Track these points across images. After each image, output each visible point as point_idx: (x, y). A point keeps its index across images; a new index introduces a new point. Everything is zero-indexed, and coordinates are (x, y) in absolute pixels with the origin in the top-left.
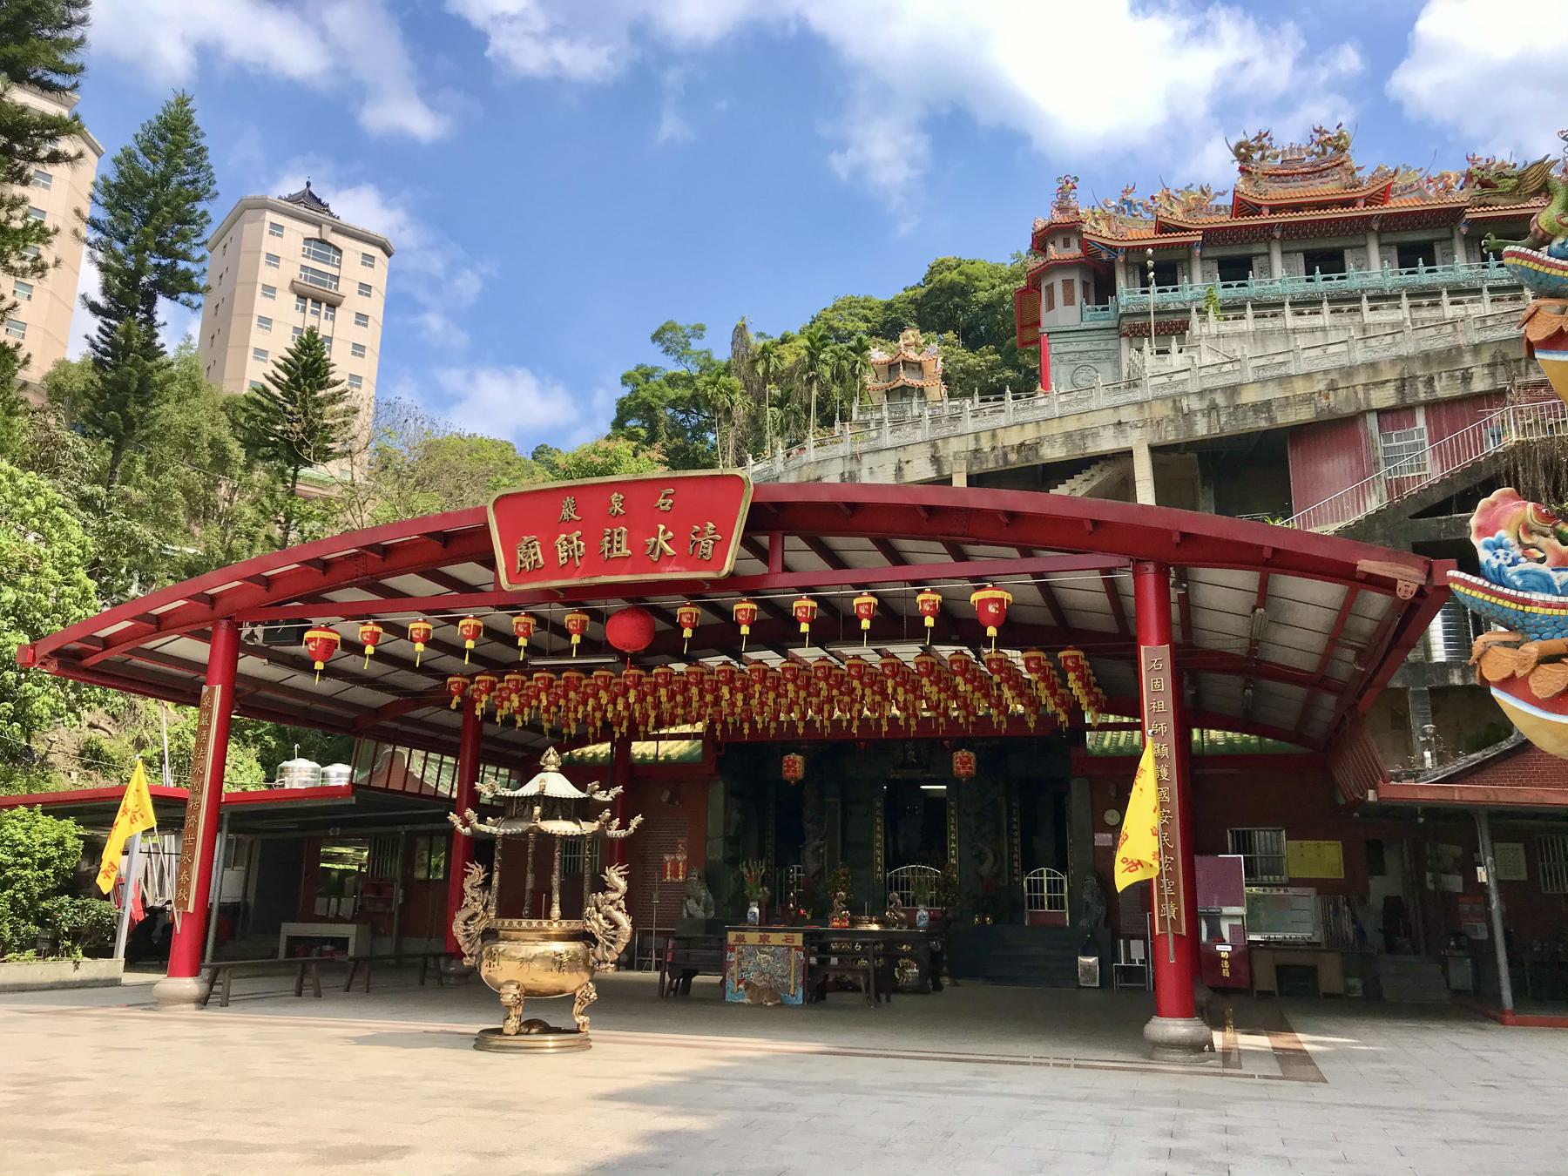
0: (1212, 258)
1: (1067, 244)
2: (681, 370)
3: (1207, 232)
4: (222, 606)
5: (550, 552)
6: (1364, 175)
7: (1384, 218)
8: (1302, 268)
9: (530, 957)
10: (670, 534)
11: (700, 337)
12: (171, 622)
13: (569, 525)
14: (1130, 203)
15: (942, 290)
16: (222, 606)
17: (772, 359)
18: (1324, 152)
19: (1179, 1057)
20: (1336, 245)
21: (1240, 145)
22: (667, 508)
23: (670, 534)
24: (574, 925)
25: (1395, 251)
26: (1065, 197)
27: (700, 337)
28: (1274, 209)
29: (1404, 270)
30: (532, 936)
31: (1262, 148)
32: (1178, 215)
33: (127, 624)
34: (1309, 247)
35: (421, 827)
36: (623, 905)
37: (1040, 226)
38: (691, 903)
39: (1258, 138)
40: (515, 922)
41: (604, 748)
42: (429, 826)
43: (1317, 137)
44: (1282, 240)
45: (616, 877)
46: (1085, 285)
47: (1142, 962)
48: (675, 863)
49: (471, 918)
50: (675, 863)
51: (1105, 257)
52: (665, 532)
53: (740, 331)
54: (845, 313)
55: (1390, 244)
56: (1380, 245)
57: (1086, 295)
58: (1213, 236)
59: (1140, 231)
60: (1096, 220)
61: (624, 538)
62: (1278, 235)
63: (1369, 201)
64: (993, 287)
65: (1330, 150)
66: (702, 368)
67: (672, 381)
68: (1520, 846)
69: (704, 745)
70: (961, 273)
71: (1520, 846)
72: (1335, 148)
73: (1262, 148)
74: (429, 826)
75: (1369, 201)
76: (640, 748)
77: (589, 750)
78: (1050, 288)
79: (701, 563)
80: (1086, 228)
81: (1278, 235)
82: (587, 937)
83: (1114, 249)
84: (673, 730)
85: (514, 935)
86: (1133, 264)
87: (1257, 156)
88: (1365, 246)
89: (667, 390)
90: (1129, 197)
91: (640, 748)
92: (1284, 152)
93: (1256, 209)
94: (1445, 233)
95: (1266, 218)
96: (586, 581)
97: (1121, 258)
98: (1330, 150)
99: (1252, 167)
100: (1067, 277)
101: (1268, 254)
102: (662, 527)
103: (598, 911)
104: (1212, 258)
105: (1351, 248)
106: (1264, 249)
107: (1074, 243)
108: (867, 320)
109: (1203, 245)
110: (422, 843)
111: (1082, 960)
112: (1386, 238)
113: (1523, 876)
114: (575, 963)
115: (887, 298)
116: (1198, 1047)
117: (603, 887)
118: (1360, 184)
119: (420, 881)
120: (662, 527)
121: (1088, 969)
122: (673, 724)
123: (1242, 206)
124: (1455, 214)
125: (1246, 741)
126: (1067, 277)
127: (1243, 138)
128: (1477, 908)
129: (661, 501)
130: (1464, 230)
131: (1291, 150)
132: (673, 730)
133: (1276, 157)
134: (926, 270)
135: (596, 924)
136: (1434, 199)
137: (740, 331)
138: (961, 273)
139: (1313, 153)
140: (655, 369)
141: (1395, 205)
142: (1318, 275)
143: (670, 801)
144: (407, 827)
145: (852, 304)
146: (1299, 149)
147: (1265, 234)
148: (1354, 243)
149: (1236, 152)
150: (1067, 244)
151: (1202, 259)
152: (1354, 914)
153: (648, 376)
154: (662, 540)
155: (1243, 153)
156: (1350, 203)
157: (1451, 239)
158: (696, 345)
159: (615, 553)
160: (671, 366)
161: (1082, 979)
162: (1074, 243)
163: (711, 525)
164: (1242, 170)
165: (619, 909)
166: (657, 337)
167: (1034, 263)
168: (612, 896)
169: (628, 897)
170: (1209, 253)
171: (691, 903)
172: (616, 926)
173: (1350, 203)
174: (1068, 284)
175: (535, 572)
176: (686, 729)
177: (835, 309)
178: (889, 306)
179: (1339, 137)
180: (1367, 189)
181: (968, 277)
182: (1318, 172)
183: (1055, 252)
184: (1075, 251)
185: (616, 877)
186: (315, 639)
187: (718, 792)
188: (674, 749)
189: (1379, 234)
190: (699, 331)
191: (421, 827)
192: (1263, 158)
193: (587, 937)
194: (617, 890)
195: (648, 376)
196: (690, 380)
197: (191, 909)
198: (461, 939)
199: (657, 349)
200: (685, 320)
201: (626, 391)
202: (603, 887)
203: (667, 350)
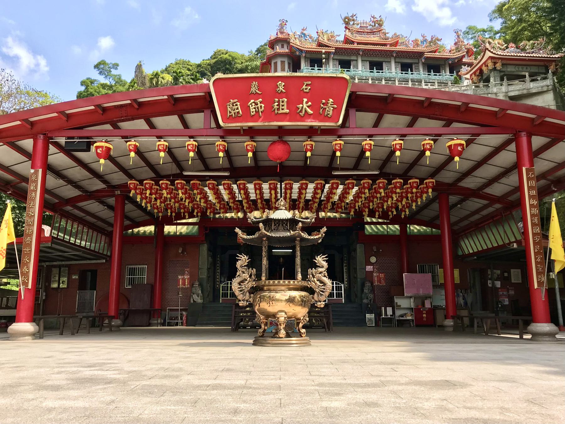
0: (336, 59)
1: (283, 47)
2: (107, 82)
3: (336, 48)
4: (37, 128)
5: (246, 108)
6: (390, 35)
7: (398, 52)
8: (368, 67)
9: (283, 301)
10: (310, 103)
11: (116, 69)
12: (4, 134)
13: (256, 96)
14: (304, 34)
15: (222, 62)
16: (37, 128)
17: (160, 79)
18: (375, 25)
19: (547, 339)
20: (381, 60)
21: (346, 18)
22: (307, 91)
23: (310, 103)
24: (305, 284)
25: (400, 65)
26: (282, 28)
27: (116, 69)
28: (358, 43)
29: (404, 72)
30: (283, 288)
31: (353, 20)
32: (325, 41)
33: (18, 123)
34: (371, 59)
35: (55, 263)
36: (326, 275)
37: (272, 38)
38: (195, 296)
39: (352, 16)
40: (276, 282)
41: (150, 229)
42: (60, 263)
43: (372, 19)
44: (362, 56)
45: (321, 260)
46: (289, 64)
47: (391, 315)
48: (184, 280)
49: (242, 282)
50: (184, 280)
51: (297, 53)
52: (307, 103)
53: (139, 68)
54: (181, 66)
55: (398, 62)
56: (395, 62)
57: (289, 68)
58: (338, 51)
59: (311, 46)
60: (295, 38)
61: (285, 104)
62: (361, 53)
63: (391, 45)
64: (242, 63)
65: (377, 25)
66: (116, 82)
67: (104, 86)
68: (519, 270)
69: (199, 228)
70: (230, 56)
71: (519, 270)
72: (379, 24)
73: (353, 20)
74: (60, 263)
75: (391, 45)
76: (169, 229)
77: (142, 229)
78: (276, 64)
79: (326, 118)
80: (291, 41)
81: (361, 53)
82: (311, 291)
83: (301, 51)
84: (184, 221)
85: (272, 288)
86: (308, 58)
87: (351, 23)
88: (390, 62)
89: (101, 89)
90: (305, 32)
91: (169, 229)
92: (361, 23)
93: (352, 42)
94: (416, 61)
95: (355, 46)
96: (266, 124)
97: (304, 55)
98: (377, 25)
99: (349, 27)
100: (283, 60)
101: (357, 60)
102: (305, 100)
103: (314, 277)
104: (336, 59)
105: (385, 62)
106: (355, 58)
107: (285, 46)
108: (189, 70)
109: (335, 54)
110: (55, 271)
111: (368, 316)
112: (398, 60)
113: (520, 282)
114: (303, 303)
115: (198, 62)
116: (551, 335)
117: (315, 266)
118: (388, 39)
119: (54, 289)
120: (305, 100)
121: (370, 320)
122: (184, 218)
123: (347, 41)
124: (421, 54)
125: (425, 231)
126: (283, 60)
127: (347, 15)
128: (505, 293)
129: (304, 87)
130: (423, 60)
131: (363, 23)
132: (184, 221)
133: (358, 24)
134: (212, 53)
135: (314, 284)
136: (411, 48)
137: (139, 68)
138: (230, 56)
139: (371, 25)
140: (95, 80)
141: (399, 48)
142: (375, 71)
143: (182, 252)
144: (47, 263)
145: (184, 62)
146: (366, 23)
147: (356, 52)
148: (386, 60)
149: (345, 21)
150: (283, 47)
151: (333, 59)
152: (464, 296)
153: (92, 83)
154: (305, 105)
155: (347, 22)
156: (385, 45)
157: (418, 63)
158: (114, 72)
159: (281, 111)
160: (102, 80)
161: (368, 323)
162: (285, 46)
163: (331, 100)
164: (346, 28)
165: (325, 276)
166: (96, 67)
167: (269, 52)
168: (320, 270)
169: (328, 270)
170: (336, 57)
171: (195, 296)
172: (325, 284)
173: (385, 45)
174: (283, 62)
175: (237, 118)
176: (190, 220)
177: (177, 64)
178: (199, 66)
179: (381, 20)
180: (390, 41)
181: (233, 58)
182: (372, 32)
183: (278, 49)
184: (286, 50)
185: (321, 260)
186: (102, 147)
187: (204, 249)
188: (183, 230)
189: (395, 58)
190: (116, 66)
191: (55, 263)
192: (354, 24)
193: (311, 291)
194: (323, 267)
195: (92, 83)
196: (111, 87)
197: (30, 287)
198: (237, 293)
199: (96, 72)
200: (110, 60)
201: (83, 88)
202: (315, 266)
203: (100, 73)
